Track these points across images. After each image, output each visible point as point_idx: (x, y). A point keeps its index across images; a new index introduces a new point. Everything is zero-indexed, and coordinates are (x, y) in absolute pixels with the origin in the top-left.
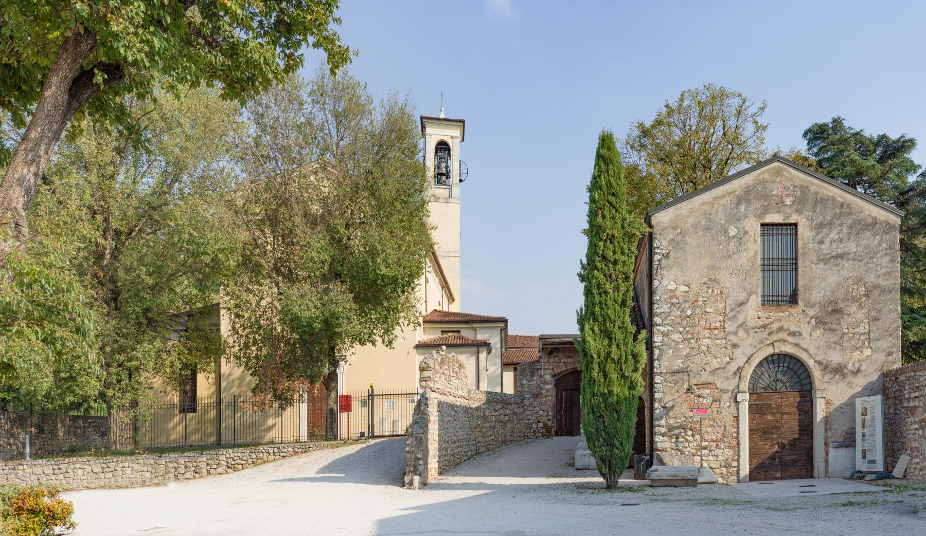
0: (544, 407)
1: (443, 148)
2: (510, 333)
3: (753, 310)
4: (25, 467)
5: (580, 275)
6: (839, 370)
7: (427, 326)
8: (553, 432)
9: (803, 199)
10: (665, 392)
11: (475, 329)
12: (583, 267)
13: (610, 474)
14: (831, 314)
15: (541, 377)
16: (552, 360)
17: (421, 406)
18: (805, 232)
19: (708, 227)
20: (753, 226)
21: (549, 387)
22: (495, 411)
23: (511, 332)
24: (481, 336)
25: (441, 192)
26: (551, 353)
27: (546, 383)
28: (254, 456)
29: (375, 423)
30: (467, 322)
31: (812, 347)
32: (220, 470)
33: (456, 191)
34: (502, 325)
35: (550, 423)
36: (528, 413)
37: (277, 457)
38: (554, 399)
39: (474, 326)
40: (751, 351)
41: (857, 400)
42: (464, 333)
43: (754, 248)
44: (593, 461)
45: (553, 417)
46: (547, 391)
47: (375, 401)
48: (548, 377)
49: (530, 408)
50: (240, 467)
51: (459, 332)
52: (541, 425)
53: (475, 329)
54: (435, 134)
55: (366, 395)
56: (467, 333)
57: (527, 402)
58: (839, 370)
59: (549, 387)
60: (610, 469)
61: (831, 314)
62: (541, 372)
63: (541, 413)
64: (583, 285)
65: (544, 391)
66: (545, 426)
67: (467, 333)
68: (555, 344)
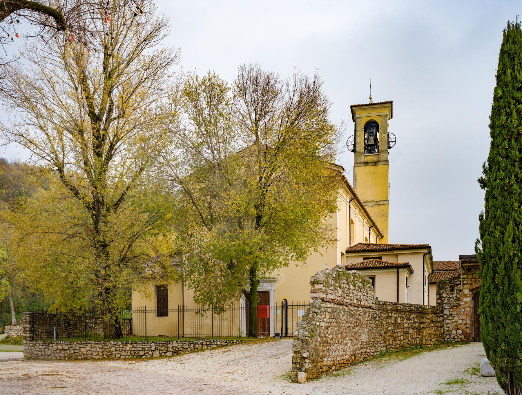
0: (463, 317)
2: (435, 260)
4: (54, 345)
5: (481, 181)
7: (349, 255)
8: (471, 339)
11: (397, 255)
12: (485, 171)
13: (512, 387)
15: (461, 291)
16: (470, 276)
21: (468, 299)
22: (409, 319)
23: (437, 257)
24: (402, 260)
26: (469, 270)
27: (465, 296)
28: (192, 346)
29: (288, 326)
30: (389, 250)
32: (168, 354)
34: (426, 251)
35: (468, 331)
36: (447, 321)
37: (209, 348)
38: (472, 310)
39: (396, 252)
42: (384, 259)
44: (493, 371)
45: (471, 325)
46: (466, 303)
47: (288, 310)
48: (466, 291)
49: (450, 318)
50: (182, 353)
51: (381, 258)
52: (460, 332)
53: (397, 255)
55: (280, 305)
56: (388, 259)
57: (446, 312)
59: (468, 299)
60: (512, 382)
62: (460, 287)
63: (460, 321)
64: (484, 192)
65: (462, 303)
66: (464, 332)
67: (388, 259)
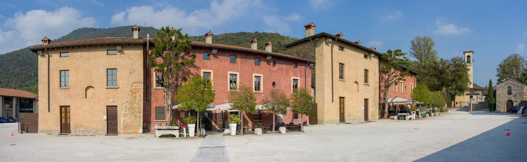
1: (469, 57)
3: (507, 95)
6: (516, 101)
9: (512, 84)
10: (497, 103)
14: (515, 96)
17: (470, 104)
18: (512, 87)
19: (502, 87)
20: (507, 87)
25: (469, 64)
31: (513, 99)
33: (472, 64)
40: (506, 100)
41: (42, 61)
43: (507, 89)
54: (467, 54)
58: (516, 101)
61: (515, 96)
68: (199, 122)
